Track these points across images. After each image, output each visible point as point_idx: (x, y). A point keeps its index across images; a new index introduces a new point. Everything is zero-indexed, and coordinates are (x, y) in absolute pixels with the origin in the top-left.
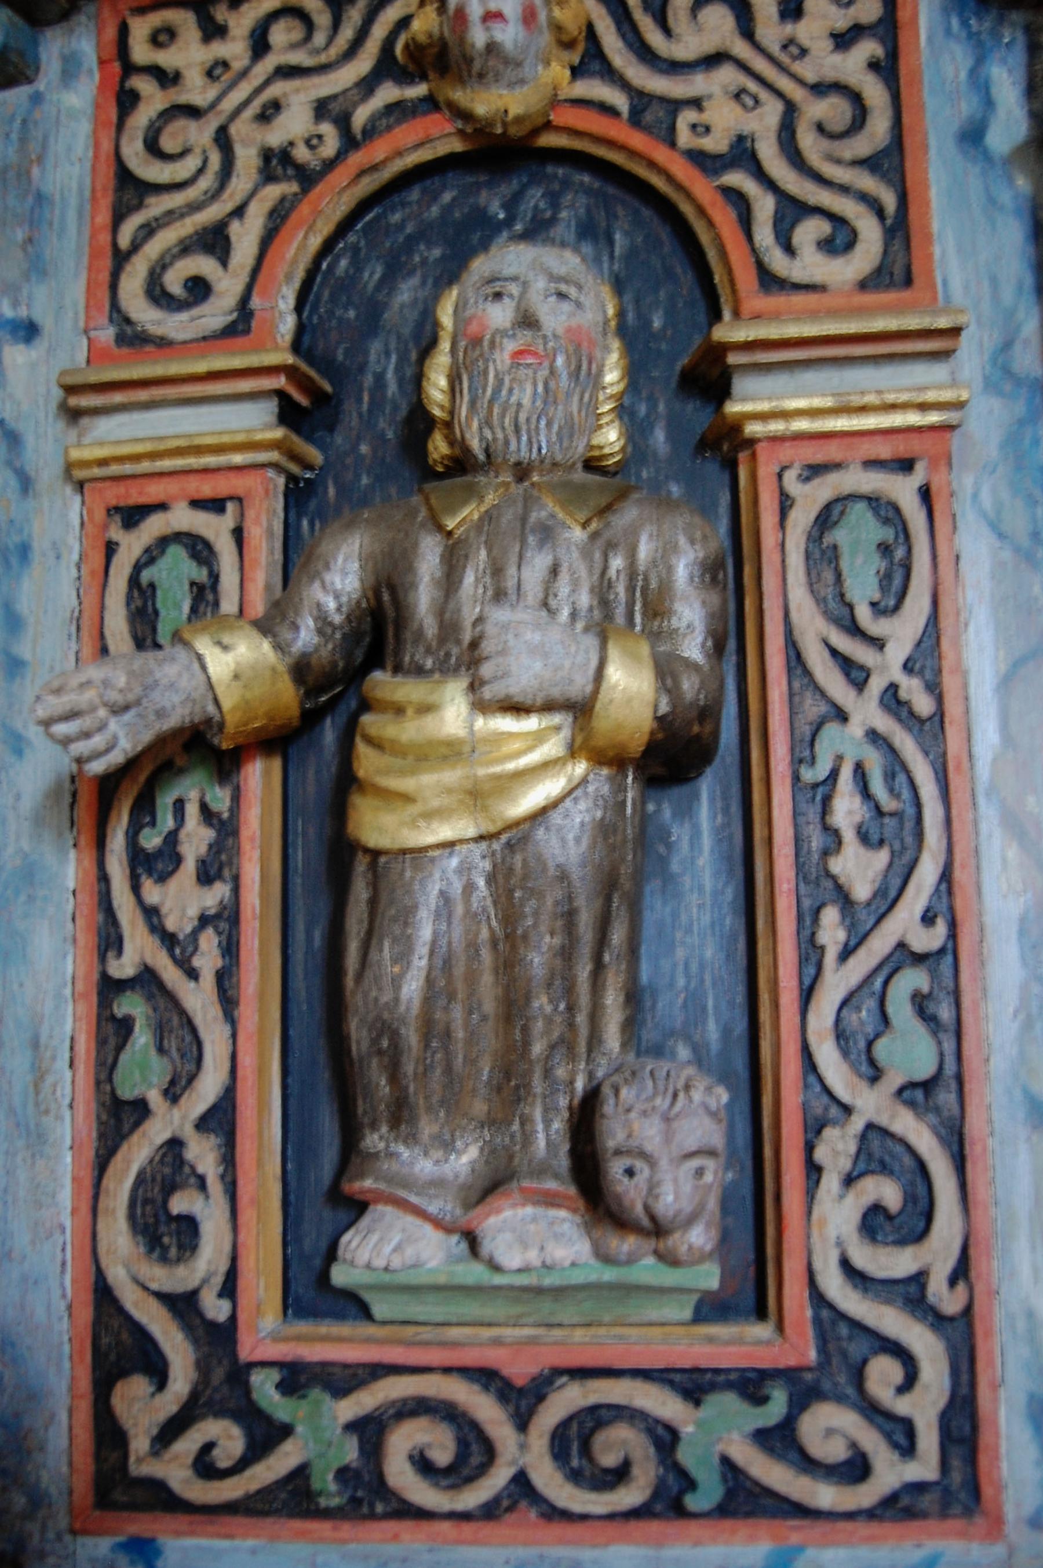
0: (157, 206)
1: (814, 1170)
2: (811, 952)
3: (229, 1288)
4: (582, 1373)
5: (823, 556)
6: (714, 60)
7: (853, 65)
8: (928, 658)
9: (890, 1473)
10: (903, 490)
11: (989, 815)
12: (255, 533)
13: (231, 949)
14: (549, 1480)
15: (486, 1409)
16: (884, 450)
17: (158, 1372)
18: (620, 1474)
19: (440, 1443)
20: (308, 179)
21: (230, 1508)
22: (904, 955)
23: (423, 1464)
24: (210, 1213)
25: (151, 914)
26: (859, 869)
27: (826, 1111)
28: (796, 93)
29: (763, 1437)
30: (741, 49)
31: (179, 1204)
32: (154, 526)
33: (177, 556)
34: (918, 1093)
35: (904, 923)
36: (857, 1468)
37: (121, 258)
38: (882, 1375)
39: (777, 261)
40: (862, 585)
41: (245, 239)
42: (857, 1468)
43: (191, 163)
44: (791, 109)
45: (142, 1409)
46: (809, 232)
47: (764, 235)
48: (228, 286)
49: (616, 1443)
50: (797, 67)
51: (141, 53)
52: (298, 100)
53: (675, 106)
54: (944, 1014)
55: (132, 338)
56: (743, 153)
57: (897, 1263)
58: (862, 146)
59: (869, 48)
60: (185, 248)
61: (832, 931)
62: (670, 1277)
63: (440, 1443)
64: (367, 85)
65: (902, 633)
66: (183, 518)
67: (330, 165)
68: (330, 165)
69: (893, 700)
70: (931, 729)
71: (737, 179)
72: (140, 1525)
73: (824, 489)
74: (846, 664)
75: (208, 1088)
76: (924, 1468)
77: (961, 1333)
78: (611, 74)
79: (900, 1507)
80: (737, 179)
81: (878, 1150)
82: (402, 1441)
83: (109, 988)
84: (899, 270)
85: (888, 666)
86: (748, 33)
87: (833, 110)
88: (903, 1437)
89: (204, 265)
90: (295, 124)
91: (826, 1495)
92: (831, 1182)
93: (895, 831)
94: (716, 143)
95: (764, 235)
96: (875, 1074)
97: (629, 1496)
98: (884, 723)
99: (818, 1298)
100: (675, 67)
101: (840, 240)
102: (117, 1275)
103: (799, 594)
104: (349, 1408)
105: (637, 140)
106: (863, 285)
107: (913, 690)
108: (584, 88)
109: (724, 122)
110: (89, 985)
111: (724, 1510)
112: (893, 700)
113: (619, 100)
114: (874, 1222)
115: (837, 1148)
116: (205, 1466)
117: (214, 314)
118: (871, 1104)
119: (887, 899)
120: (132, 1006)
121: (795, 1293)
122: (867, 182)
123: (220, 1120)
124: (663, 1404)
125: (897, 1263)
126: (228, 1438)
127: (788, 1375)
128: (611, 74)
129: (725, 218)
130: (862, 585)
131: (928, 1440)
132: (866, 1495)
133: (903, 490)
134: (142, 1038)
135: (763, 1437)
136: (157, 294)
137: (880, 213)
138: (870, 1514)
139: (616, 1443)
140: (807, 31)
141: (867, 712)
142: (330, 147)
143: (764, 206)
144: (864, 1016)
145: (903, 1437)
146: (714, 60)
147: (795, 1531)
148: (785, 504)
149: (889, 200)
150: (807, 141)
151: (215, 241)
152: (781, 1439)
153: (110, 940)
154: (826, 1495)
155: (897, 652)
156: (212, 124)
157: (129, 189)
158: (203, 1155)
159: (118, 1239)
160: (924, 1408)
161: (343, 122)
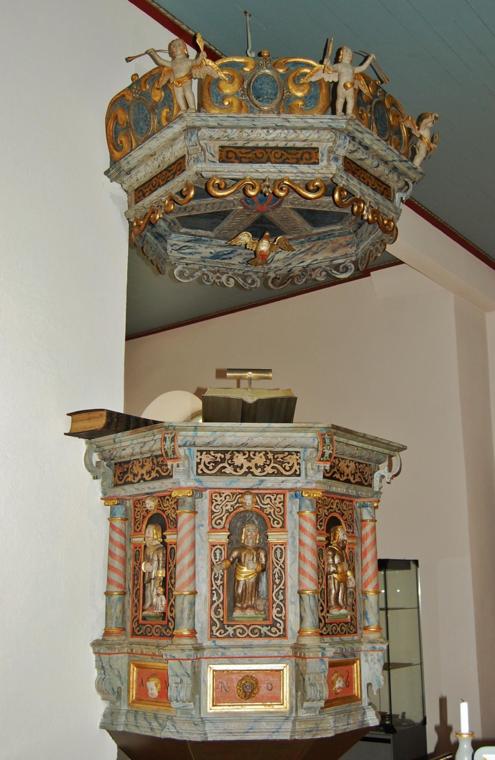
0: (216, 514)
1: (273, 607)
2: (273, 588)
3: (223, 618)
4: (253, 625)
5: (275, 553)
6: (267, 504)
7: (280, 505)
8: (284, 563)
9: (278, 633)
10: (282, 547)
11: (288, 576)
12: (226, 548)
13: (223, 587)
14: (250, 634)
15: (245, 628)
18: (256, 633)
20: (230, 513)
21: (222, 638)
23: (240, 633)
24: (221, 611)
25: (216, 584)
26: (277, 581)
27: (274, 602)
29: (268, 630)
30: (270, 503)
31: (218, 610)
32: (216, 547)
34: (281, 601)
35: (281, 586)
36: (276, 633)
37: (212, 519)
38: (278, 625)
39: (273, 525)
40: (279, 556)
41: (224, 518)
42: (276, 633)
43: (218, 511)
45: (214, 629)
46: (276, 522)
47: (272, 522)
48: (223, 523)
49: (256, 631)
51: (214, 498)
52: (229, 504)
53: (264, 508)
54: (284, 594)
55: (213, 528)
56: (270, 514)
57: (279, 615)
58: (281, 514)
59: (282, 504)
60: (218, 519)
61: (275, 587)
62: (261, 616)
63: (276, 155)
64: (236, 503)
65: (282, 560)
66: (218, 547)
67: (232, 512)
68: (232, 512)
69: (278, 564)
70: (284, 569)
72: (214, 639)
73: (276, 547)
74: (277, 563)
75: (221, 600)
76: (281, 633)
77: (284, 621)
78: (258, 504)
79: (279, 636)
81: (278, 606)
82: (238, 631)
83: (212, 590)
84: (283, 527)
85: (281, 563)
86: (271, 501)
87: (278, 510)
88: (280, 631)
89: (220, 521)
90: (229, 507)
91: (273, 635)
92: (274, 608)
93: (280, 578)
94: (268, 513)
95: (272, 522)
96: (278, 599)
97: (257, 635)
98: (280, 568)
99: (273, 618)
100: (165, 507)
101: (278, 524)
102: (212, 617)
103: (273, 556)
104: (233, 628)
105: (261, 512)
106: (280, 528)
107: (282, 566)
108: (256, 506)
109: (269, 510)
110: (210, 590)
111: (265, 637)
112: (281, 566)
113: (259, 507)
114: (278, 612)
115: (275, 605)
117: (222, 526)
118: (278, 602)
119: (279, 584)
120: (214, 592)
121: (271, 618)
122: (281, 517)
123: (222, 603)
124: (260, 627)
125: (279, 615)
126: (223, 631)
127: (270, 625)
128: (258, 504)
129: (268, 520)
130: (279, 556)
131: (282, 631)
132: (277, 635)
133: (282, 547)
134: (215, 595)
135: (268, 630)
136: (216, 524)
139: (256, 631)
140: (276, 502)
141: (278, 567)
142: (232, 510)
143: (272, 519)
144: (277, 594)
145: (280, 631)
146: (267, 504)
147: (271, 638)
148: (272, 548)
150: (276, 513)
151: (221, 519)
152: (270, 631)
153: (212, 586)
154: (273, 635)
155: (281, 562)
156: (221, 506)
157: (213, 512)
158: (221, 606)
159: (213, 613)
160: (281, 628)
161: (233, 507)
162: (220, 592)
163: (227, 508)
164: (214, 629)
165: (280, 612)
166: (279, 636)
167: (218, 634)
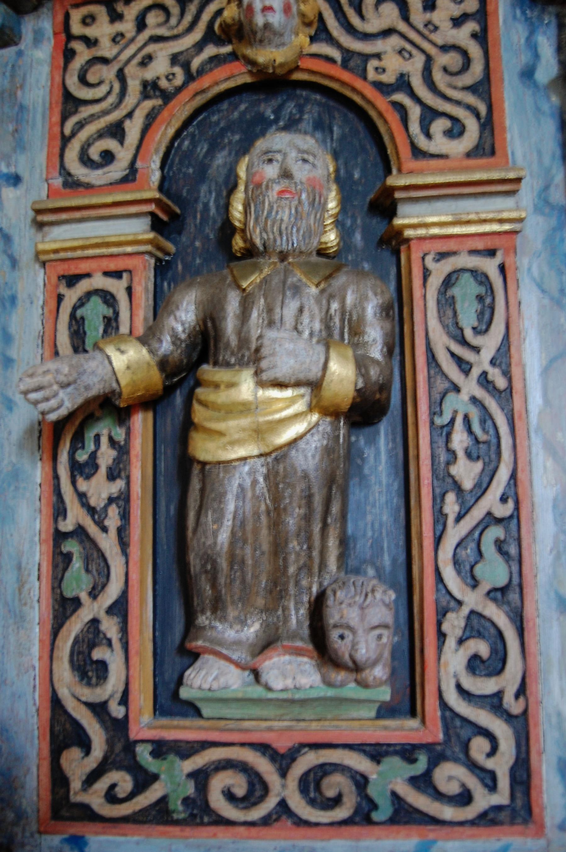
0: (85, 112)
1: (442, 636)
2: (440, 517)
3: (124, 700)
4: (316, 746)
5: (447, 302)
6: (387, 32)
7: (463, 35)
8: (503, 357)
9: (483, 800)
10: (490, 267)
11: (537, 443)
12: (138, 290)
13: (125, 516)
14: (298, 804)
15: (264, 766)
16: (480, 245)
17: (86, 745)
18: (337, 801)
19: (239, 784)
20: (167, 97)
21: (125, 820)
22: (490, 519)
23: (230, 796)
24: (114, 659)
25: (82, 497)
26: (466, 472)
27: (448, 604)
28: (432, 51)
29: (414, 781)
30: (402, 26)
31: (97, 654)
32: (84, 286)
33: (96, 302)
34: (498, 594)
35: (491, 502)
36: (465, 798)
37: (66, 140)
38: (479, 747)
39: (422, 142)
40: (468, 318)
41: (133, 130)
42: (465, 798)
43: (104, 89)
44: (429, 59)
45: (77, 765)
46: (439, 126)
47: (415, 128)
48: (124, 155)
49: (334, 784)
50: (433, 37)
51: (76, 29)
53: (366, 57)
54: (512, 551)
55: (72, 184)
56: (403, 83)
57: (487, 686)
58: (468, 79)
59: (471, 26)
60: (101, 135)
61: (451, 506)
62: (363, 694)
63: (239, 784)
64: (199, 46)
65: (490, 344)
66: (99, 281)
67: (179, 90)
68: (179, 90)
70: (505, 396)
71: (400, 97)
72: (76, 829)
73: (447, 266)
74: (459, 361)
75: (113, 591)
76: (502, 797)
77: (522, 724)
78: (331, 40)
79: (488, 819)
80: (400, 97)
81: (476, 625)
82: (218, 783)
83: (59, 537)
84: (488, 147)
85: (482, 362)
86: (406, 18)
87: (452, 60)
89: (111, 144)
90: (160, 67)
91: (448, 812)
92: (451, 643)
93: (486, 451)
94: (389, 78)
95: (415, 128)
96: (475, 584)
97: (342, 813)
98: (480, 393)
99: (444, 705)
101: (456, 130)
102: (64, 693)
103: (433, 323)
104: (189, 765)
105: (346, 76)
106: (468, 155)
107: (495, 375)
108: (317, 48)
109: (393, 66)
110: (48, 535)
111: (393, 821)
112: (484, 380)
113: (336, 54)
116: (111, 797)
117: (116, 171)
118: (473, 600)
119: (482, 489)
120: (72, 547)
122: (471, 99)
123: (120, 609)
124: (360, 763)
125: (487, 686)
126: (124, 781)
127: (428, 747)
128: (331, 40)
129: (393, 118)
130: (468, 318)
131: (504, 782)
132: (470, 812)
133: (490, 267)
135: (414, 781)
136: (85, 160)
137: (478, 116)
138: (472, 823)
139: (334, 784)
140: (438, 17)
141: (470, 387)
142: (179, 80)
143: (415, 112)
144: (469, 552)
145: (490, 781)
146: (387, 32)
147: (431, 832)
148: (426, 274)
149: (483, 109)
150: (438, 77)
151: (117, 131)
152: (424, 782)
153: (60, 511)
154: (448, 812)
155: (487, 354)
156: (115, 67)
157: (70, 103)
158: (110, 627)
159: (64, 673)
160: (502, 765)
161: (186, 66)
162: (108, 543)
163: (149, 74)
164: (77, 765)
165: (495, 664)
166: (488, 819)
167: (95, 799)
